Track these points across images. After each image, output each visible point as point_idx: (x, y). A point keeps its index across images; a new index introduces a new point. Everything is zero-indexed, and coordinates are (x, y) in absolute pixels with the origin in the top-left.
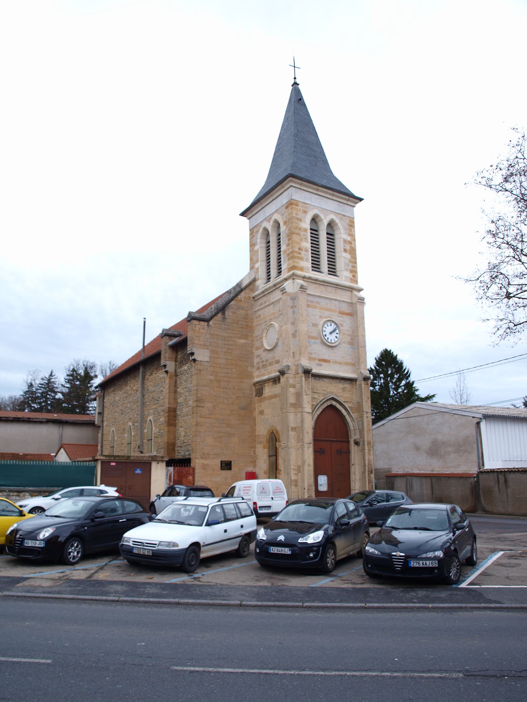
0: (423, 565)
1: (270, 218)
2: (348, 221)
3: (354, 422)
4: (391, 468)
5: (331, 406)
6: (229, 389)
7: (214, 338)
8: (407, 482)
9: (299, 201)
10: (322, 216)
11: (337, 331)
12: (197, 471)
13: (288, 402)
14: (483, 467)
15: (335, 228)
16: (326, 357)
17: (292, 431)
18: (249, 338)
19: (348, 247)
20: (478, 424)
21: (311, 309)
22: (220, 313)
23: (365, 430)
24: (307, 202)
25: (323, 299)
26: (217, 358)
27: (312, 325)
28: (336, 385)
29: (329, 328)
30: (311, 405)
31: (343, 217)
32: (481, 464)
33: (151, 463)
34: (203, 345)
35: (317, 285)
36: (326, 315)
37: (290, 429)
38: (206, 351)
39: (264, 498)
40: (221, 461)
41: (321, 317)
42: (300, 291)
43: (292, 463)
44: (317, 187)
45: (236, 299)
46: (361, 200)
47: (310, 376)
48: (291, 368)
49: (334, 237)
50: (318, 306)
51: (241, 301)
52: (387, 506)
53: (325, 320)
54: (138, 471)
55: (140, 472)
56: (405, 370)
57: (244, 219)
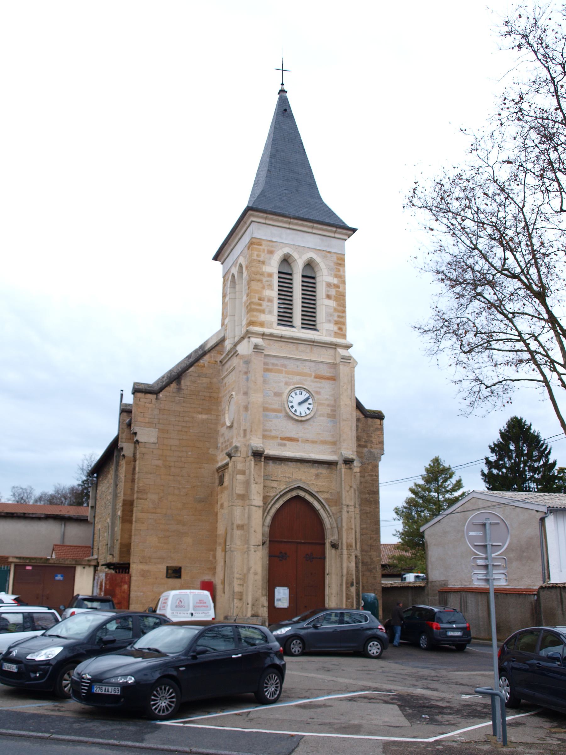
0: (105, 691)
1: (237, 263)
2: (334, 259)
3: (331, 518)
4: (447, 581)
5: (298, 497)
6: (182, 476)
7: (164, 414)
8: (461, 599)
9: (264, 240)
10: (295, 255)
11: (310, 401)
12: (134, 578)
13: (234, 493)
14: (548, 580)
15: (316, 270)
16: (293, 435)
17: (238, 529)
18: (213, 413)
19: (333, 292)
20: (542, 520)
21: (273, 374)
22: (174, 382)
23: (344, 529)
24: (274, 240)
25: (292, 361)
26: (167, 438)
27: (273, 394)
28: (305, 470)
29: (297, 398)
30: (262, 497)
31: (328, 254)
32: (546, 577)
33: (75, 568)
34: (149, 423)
35: (283, 344)
36: (295, 381)
37: (235, 527)
38: (153, 429)
39: (180, 613)
40: (167, 567)
41: (287, 384)
42: (253, 353)
43: (236, 571)
44: (289, 220)
45: (197, 364)
46: (354, 230)
47: (263, 460)
48: (240, 449)
49: (316, 280)
50: (284, 369)
51: (204, 366)
52: (339, 630)
53: (292, 387)
54: (59, 577)
55: (61, 578)
56: (543, 444)
57: (218, 263)
